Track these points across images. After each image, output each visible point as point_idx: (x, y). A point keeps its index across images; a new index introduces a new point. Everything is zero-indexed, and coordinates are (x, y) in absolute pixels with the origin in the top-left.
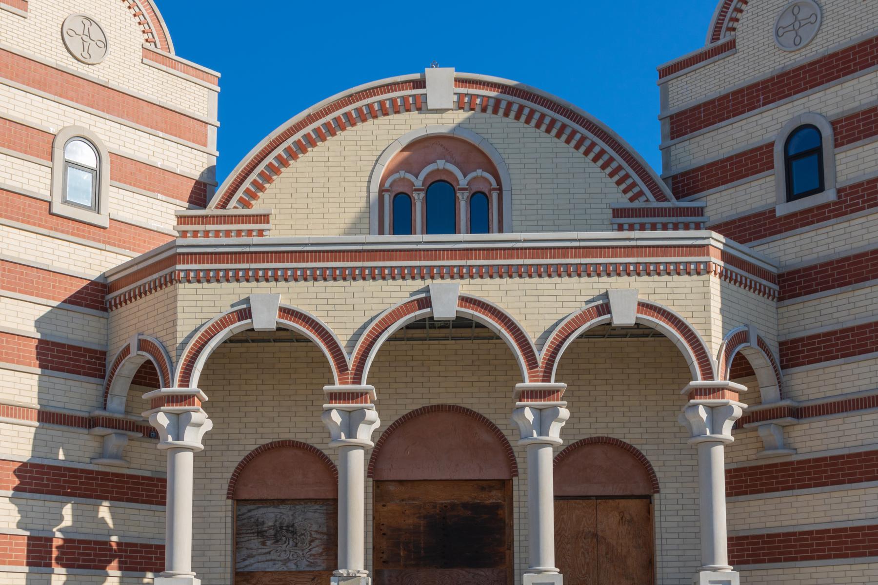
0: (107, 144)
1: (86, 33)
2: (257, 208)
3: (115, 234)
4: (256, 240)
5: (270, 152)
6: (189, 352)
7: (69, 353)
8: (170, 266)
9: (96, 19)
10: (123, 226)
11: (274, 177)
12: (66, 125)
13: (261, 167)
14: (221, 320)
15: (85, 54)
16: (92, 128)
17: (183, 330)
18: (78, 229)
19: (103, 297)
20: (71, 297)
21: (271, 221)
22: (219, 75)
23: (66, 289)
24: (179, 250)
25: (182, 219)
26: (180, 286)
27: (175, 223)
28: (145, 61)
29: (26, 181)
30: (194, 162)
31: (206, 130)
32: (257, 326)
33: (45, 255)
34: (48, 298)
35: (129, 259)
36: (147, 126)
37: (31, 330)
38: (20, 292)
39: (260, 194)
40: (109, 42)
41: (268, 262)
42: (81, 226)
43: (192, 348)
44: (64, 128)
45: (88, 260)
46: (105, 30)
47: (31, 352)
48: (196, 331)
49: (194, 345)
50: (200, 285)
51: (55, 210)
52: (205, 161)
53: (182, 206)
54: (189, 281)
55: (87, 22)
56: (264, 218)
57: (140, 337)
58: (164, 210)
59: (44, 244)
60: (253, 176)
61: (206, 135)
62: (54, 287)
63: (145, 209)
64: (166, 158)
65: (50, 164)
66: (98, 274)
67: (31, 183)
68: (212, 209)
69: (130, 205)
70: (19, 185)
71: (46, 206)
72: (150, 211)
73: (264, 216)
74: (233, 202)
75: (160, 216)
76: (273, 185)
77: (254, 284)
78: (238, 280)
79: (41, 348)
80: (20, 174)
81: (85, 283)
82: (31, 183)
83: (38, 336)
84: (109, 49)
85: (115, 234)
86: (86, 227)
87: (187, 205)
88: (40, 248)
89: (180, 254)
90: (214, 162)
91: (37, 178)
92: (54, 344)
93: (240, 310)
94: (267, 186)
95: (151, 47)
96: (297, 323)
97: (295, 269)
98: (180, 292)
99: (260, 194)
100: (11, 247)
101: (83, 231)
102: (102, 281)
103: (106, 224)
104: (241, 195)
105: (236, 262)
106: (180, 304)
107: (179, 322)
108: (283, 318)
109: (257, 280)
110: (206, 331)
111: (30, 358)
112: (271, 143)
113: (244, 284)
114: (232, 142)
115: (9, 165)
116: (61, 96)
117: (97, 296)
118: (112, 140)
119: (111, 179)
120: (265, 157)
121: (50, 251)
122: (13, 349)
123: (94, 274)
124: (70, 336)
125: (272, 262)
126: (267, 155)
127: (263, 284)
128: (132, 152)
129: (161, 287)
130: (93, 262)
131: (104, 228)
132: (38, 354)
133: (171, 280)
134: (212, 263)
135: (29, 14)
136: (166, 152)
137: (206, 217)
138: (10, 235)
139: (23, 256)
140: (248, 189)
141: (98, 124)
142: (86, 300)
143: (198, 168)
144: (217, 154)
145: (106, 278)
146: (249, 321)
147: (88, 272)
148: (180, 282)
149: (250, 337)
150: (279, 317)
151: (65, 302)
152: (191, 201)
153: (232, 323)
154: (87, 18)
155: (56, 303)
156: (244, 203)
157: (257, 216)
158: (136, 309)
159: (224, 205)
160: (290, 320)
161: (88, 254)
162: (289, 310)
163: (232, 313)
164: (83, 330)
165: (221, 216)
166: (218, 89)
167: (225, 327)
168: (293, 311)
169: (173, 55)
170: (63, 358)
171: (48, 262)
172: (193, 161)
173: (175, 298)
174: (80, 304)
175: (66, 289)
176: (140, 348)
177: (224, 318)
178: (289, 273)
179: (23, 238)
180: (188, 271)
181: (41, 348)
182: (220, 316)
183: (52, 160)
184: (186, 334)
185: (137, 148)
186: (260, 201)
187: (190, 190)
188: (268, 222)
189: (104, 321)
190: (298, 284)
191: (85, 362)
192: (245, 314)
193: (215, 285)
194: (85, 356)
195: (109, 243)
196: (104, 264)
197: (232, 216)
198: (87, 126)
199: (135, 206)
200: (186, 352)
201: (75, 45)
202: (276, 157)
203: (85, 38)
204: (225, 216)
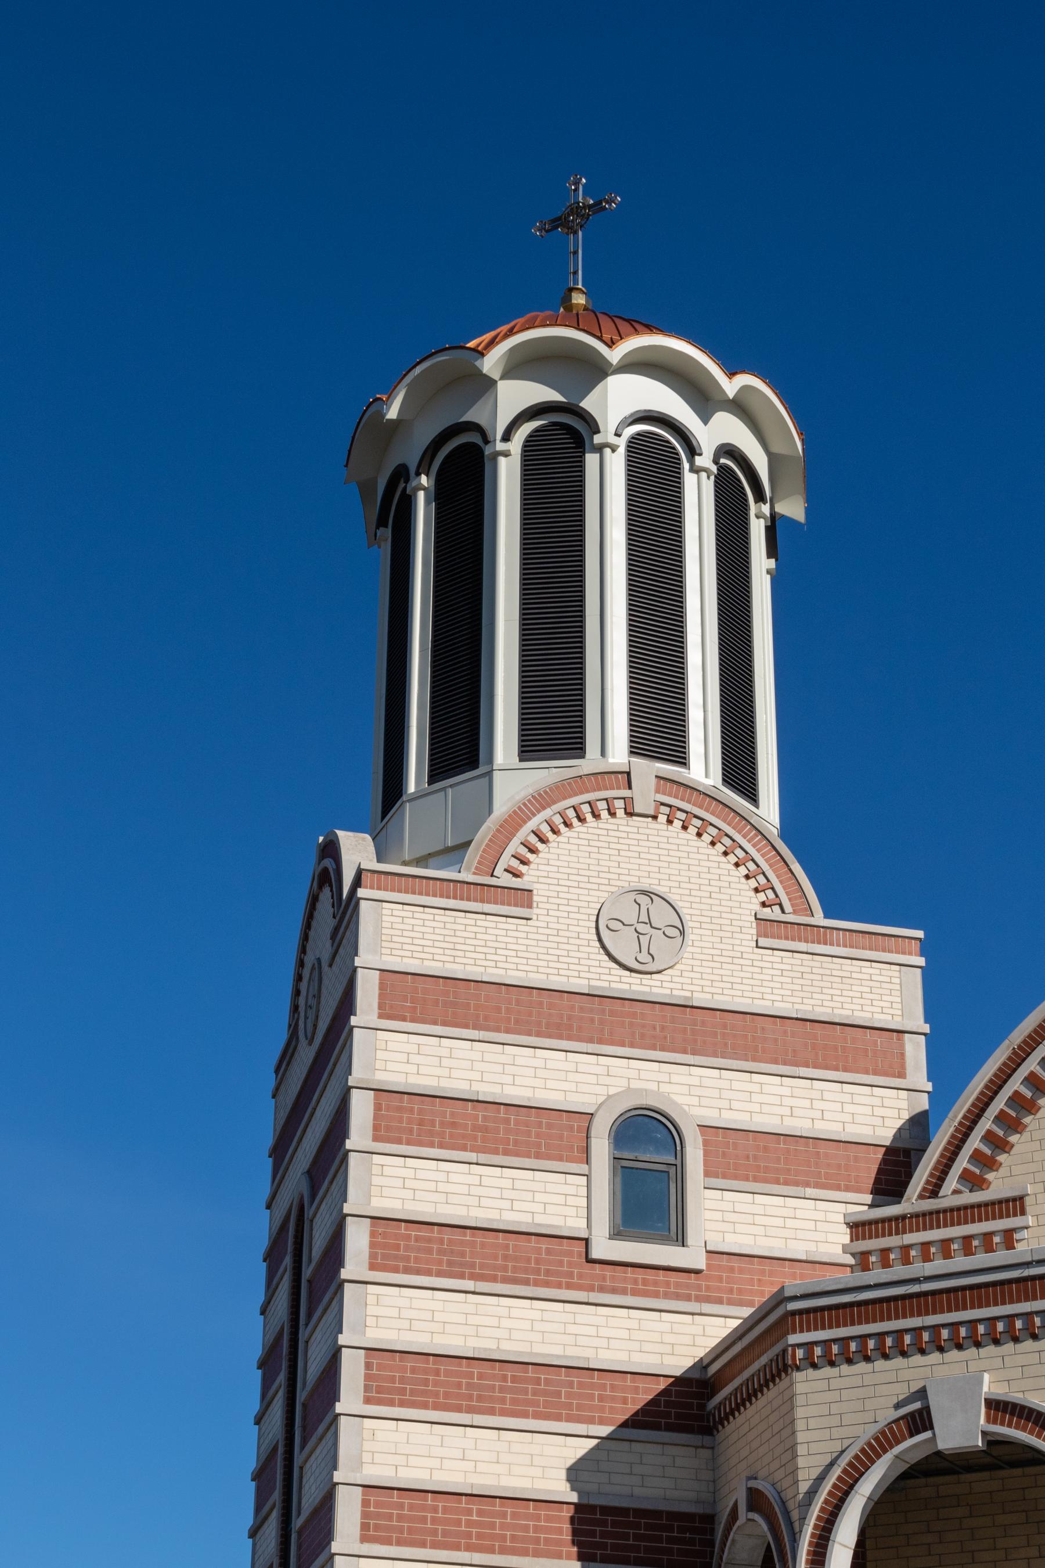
0: (696, 1111)
1: (644, 918)
2: (999, 1185)
3: (720, 1279)
4: (1001, 1257)
5: (1014, 1070)
6: (822, 1510)
7: (637, 1526)
8: (325, 1414)
9: (661, 890)
10: (736, 1263)
11: (1027, 1120)
12: (612, 1091)
13: (999, 1103)
14: (877, 1439)
15: (644, 957)
16: (665, 1088)
17: (809, 1464)
18: (645, 1282)
19: (702, 1407)
20: (636, 1414)
21: (1028, 1209)
22: (920, 934)
23: (625, 1401)
24: (792, 1306)
25: (859, 1228)
26: (798, 1376)
27: (847, 1239)
28: (763, 942)
29: (540, 1208)
30: (879, 1111)
31: (902, 1046)
32: (942, 1445)
33: (581, 1341)
34: (590, 1421)
35: (735, 1323)
36: (776, 1062)
37: (561, 1490)
38: (537, 1416)
39: (1002, 1158)
40: (688, 924)
41: (957, 1309)
42: (650, 1275)
43: (826, 1501)
44: (609, 1097)
45: (668, 1338)
46: (678, 905)
47: (560, 1531)
48: (832, 1464)
49: (830, 1493)
50: (834, 1371)
51: (597, 1252)
52: (904, 1105)
53: (859, 1203)
54: (814, 1366)
55: (643, 900)
56: (1015, 1205)
57: (752, 1484)
58: (820, 1216)
59: (579, 1319)
60: (986, 1124)
61: (902, 1055)
62: (601, 1398)
63: (779, 1222)
64: (819, 1114)
65: (584, 1168)
66: (689, 1363)
67: (550, 1209)
68: (912, 1202)
69: (749, 1219)
70: (526, 1218)
71: (580, 1247)
72: (790, 1223)
73: (1014, 1200)
74: (952, 1182)
75: (812, 1230)
76: (1026, 1135)
77: (935, 1357)
78: (904, 1354)
79: (581, 1521)
80: (529, 1196)
81: (662, 1385)
82: (550, 1209)
83: (574, 1497)
84: (690, 937)
85: (720, 1279)
86: (661, 1276)
87: (868, 1198)
88: (572, 1329)
89: (793, 1313)
90: (923, 1103)
91: (561, 1199)
92: (606, 1510)
93: (912, 1414)
94: (1013, 1139)
95: (775, 913)
96: (1024, 1430)
97: (1011, 1318)
98: (799, 1388)
99: (1002, 1158)
100: (515, 1335)
101: (656, 1283)
102: (696, 1375)
103: (701, 1263)
104: (965, 1164)
105: (897, 1318)
106: (800, 1413)
107: (801, 1450)
108: (995, 1422)
109: (941, 1349)
110: (850, 1464)
111: (559, 1543)
112: (1014, 1052)
113: (917, 1359)
114: (947, 1065)
115: (508, 1183)
116: (600, 1042)
117: (688, 1407)
118: (705, 1102)
119: (707, 1174)
120: (1005, 1082)
121: (592, 1331)
122: (526, 1528)
123: (679, 1361)
124: (637, 1491)
125: (965, 1308)
126: (1010, 1076)
127: (954, 1355)
128: (746, 1117)
129: (774, 1381)
130: (675, 1340)
131: (698, 1272)
132: (575, 1533)
133: (782, 1368)
134: (853, 1324)
135: (535, 911)
136: (817, 1104)
137: (904, 1217)
138: (514, 1313)
139: (539, 1349)
140: (977, 1152)
141: (675, 1079)
142: (668, 1415)
143: (888, 1123)
144: (929, 1087)
145: (706, 1367)
146: (927, 1434)
147: (668, 1360)
148: (798, 1369)
149: (939, 1466)
150: (988, 1420)
151: (625, 1425)
152: (876, 1191)
153: (898, 1443)
154: (644, 892)
155: (605, 1430)
156: (973, 1181)
157: (1000, 1202)
158: (746, 1428)
159: (933, 1190)
160: (1010, 1425)
161: (666, 1327)
162: (1006, 1404)
163: (896, 1421)
164: (664, 1477)
165: (931, 1213)
166: (921, 961)
167: (885, 1451)
168: (1015, 1405)
169: (819, 918)
170: (626, 1536)
171: (588, 1353)
172: (872, 1112)
173: (790, 1401)
174: (655, 1427)
175: (625, 1401)
176: (751, 1508)
177: (883, 1433)
178: (1000, 1326)
179: (537, 1315)
180: (809, 1346)
181: (581, 1521)
182: (874, 1429)
183: (588, 1162)
184: (815, 1473)
185: (756, 1108)
186: (1003, 1171)
187: (875, 1168)
188: (1023, 1213)
189: (705, 1453)
190: (983, 1351)
191: (670, 1540)
192: (920, 1421)
193: (862, 1367)
194: (670, 1529)
195: (708, 1300)
196: (700, 1341)
197: (952, 1210)
198: (653, 1087)
199: (759, 1220)
200: (815, 1511)
201: (624, 947)
202: (1026, 1079)
203: (641, 928)
204: (938, 1212)
